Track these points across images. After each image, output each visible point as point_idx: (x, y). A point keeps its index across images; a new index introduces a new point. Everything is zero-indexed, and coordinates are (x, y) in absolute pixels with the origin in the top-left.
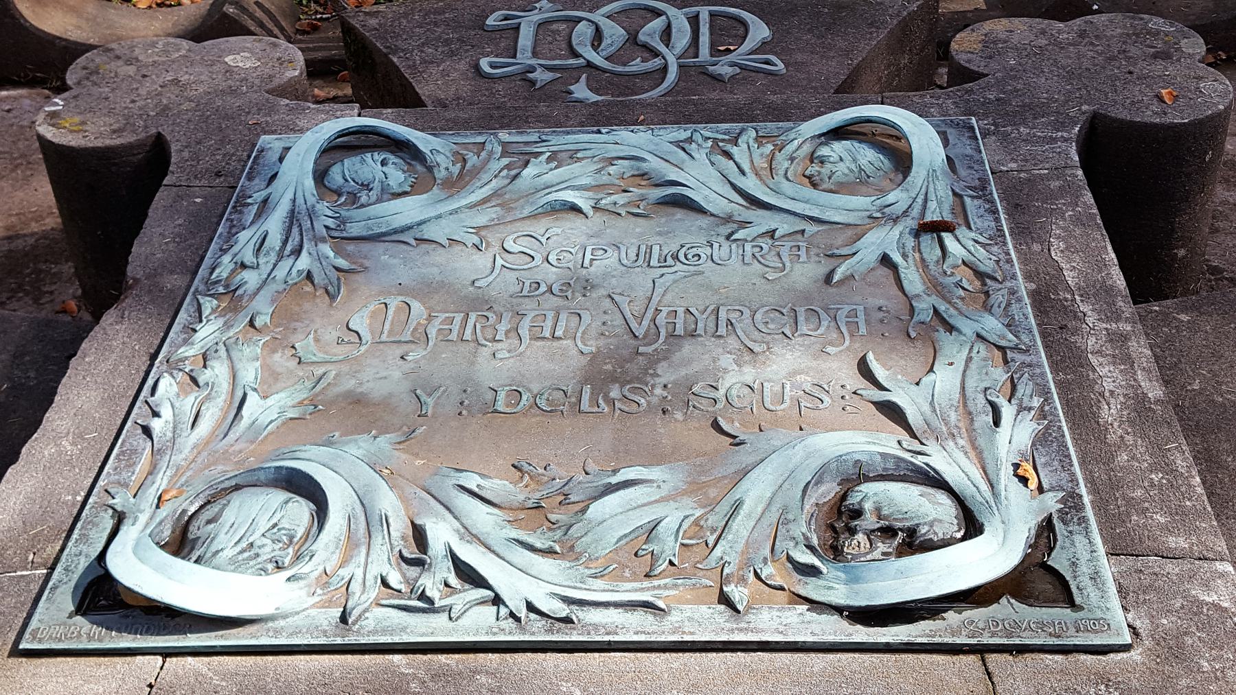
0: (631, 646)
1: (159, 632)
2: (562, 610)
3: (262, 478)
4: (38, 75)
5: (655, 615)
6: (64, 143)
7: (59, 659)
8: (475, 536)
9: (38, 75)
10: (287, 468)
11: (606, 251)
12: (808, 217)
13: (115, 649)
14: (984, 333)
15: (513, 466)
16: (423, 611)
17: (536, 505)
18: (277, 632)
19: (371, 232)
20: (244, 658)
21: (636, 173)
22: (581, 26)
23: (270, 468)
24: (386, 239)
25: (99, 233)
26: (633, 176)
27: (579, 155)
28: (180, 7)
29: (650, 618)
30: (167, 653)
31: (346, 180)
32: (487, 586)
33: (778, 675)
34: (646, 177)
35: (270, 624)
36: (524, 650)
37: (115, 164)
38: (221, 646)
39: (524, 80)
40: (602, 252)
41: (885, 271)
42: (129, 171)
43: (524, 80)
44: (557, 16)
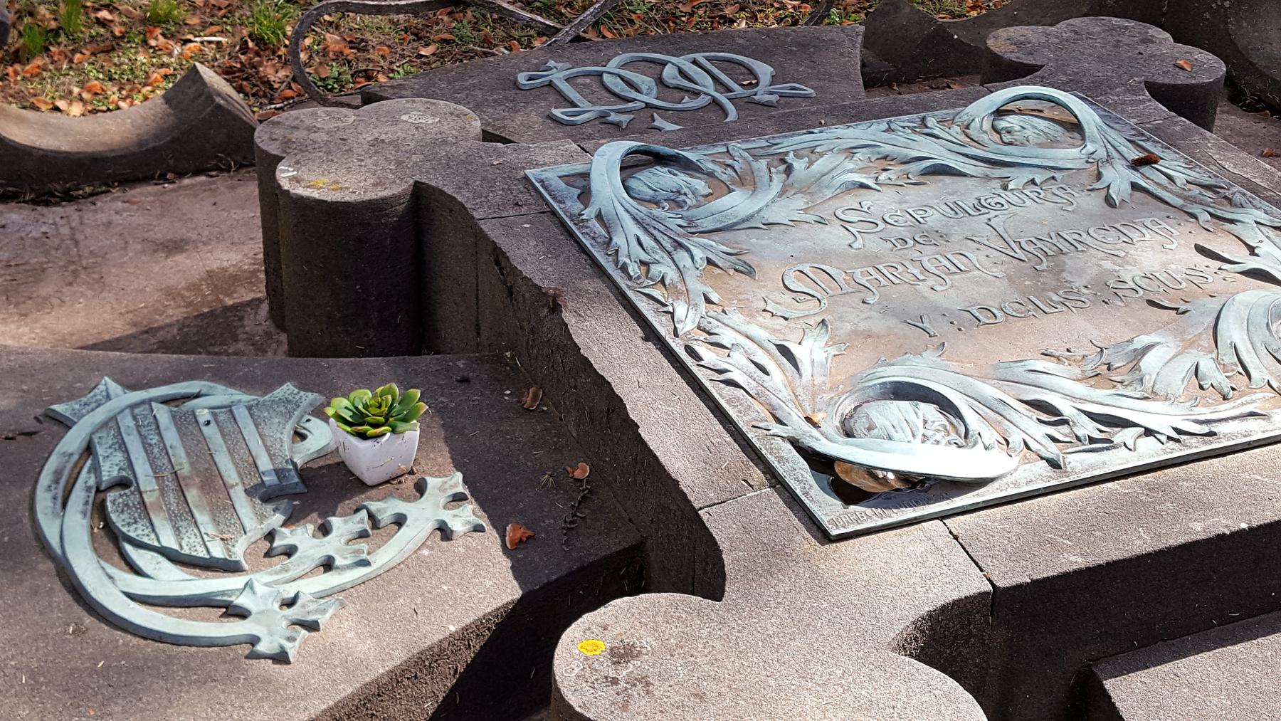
0: (1262, 443)
1: (928, 501)
2: (1205, 429)
3: (872, 394)
4: (11, 189)
5: (1264, 419)
6: (339, 200)
7: (851, 541)
8: (1080, 399)
9: (11, 189)
10: (890, 383)
11: (877, 225)
12: (1048, 167)
13: (905, 521)
14: (1258, 220)
15: (1042, 354)
16: (1107, 449)
17: (1095, 373)
18: (1015, 485)
19: (723, 224)
20: (1000, 508)
21: (879, 156)
22: (669, 67)
23: (875, 385)
24: (744, 225)
25: (358, 287)
26: (877, 159)
27: (818, 150)
28: (118, 111)
29: (1261, 421)
30: (942, 517)
31: (656, 191)
32: (1136, 425)
33: (935, 590)
34: (888, 158)
35: (1005, 480)
36: (1193, 461)
37: (386, 215)
38: (983, 502)
39: (605, 123)
40: (923, 212)
41: (1138, 195)
42: (395, 221)
43: (605, 123)
44: (577, 73)
